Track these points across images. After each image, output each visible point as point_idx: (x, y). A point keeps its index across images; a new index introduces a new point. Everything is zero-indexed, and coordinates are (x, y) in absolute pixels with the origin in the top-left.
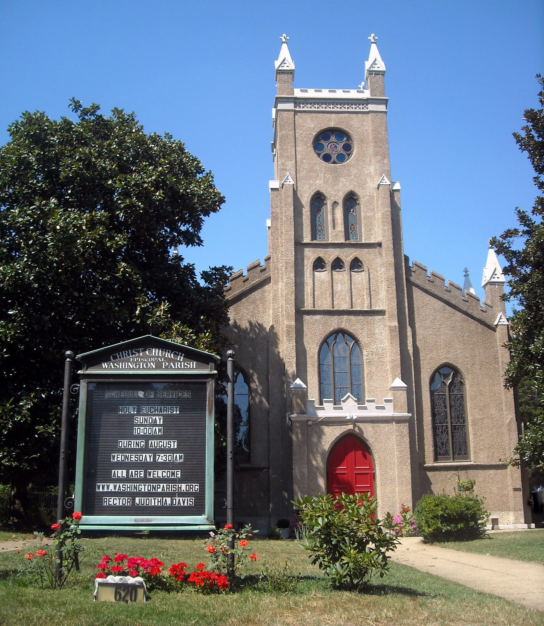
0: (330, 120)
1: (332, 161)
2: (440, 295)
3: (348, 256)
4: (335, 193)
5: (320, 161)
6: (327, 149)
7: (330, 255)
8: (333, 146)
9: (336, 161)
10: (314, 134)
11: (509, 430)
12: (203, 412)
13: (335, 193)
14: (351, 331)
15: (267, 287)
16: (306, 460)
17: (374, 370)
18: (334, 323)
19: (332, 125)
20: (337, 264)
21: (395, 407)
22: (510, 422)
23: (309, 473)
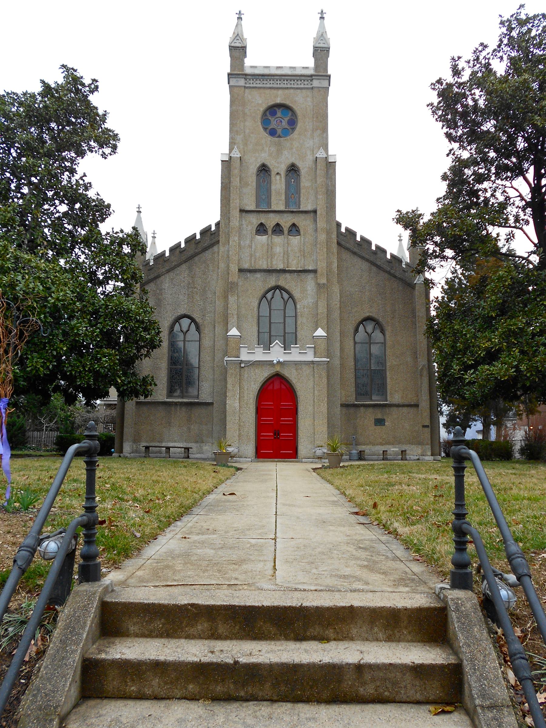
0: (276, 96)
1: (278, 134)
2: (367, 256)
4: (279, 166)
5: (265, 135)
6: (274, 124)
8: (278, 121)
9: (281, 135)
10: (262, 109)
11: (421, 375)
13: (279, 166)
14: (287, 287)
15: (215, 248)
16: (238, 396)
17: (305, 321)
18: (272, 281)
19: (278, 101)
20: (278, 229)
21: (315, 353)
22: (422, 369)
23: (240, 407)
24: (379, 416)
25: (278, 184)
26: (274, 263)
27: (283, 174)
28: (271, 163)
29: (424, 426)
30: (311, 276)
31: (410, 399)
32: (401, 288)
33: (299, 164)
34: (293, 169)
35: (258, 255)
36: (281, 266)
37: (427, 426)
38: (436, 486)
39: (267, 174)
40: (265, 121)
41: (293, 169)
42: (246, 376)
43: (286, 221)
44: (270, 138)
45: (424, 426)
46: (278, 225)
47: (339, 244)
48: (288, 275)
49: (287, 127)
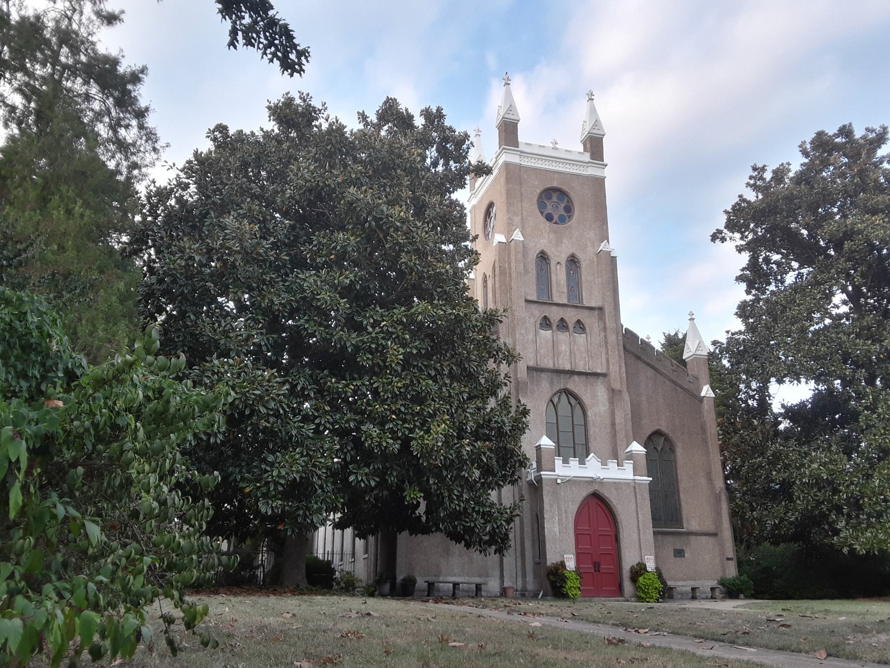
1: (554, 221)
3: (571, 316)
4: (559, 256)
5: (542, 219)
6: (549, 209)
7: (555, 314)
12: (304, 584)
13: (559, 256)
20: (563, 325)
24: (678, 547)
25: (559, 275)
26: (560, 362)
27: (563, 263)
28: (550, 252)
29: (728, 559)
30: (601, 379)
31: (709, 527)
32: (688, 400)
33: (579, 255)
34: (573, 261)
35: (542, 351)
36: (568, 367)
37: (732, 559)
38: (833, 631)
39: (574, 266)
40: (541, 206)
41: (573, 261)
42: (562, 494)
43: (571, 316)
44: (548, 223)
45: (728, 559)
46: (562, 320)
47: (625, 348)
48: (576, 378)
49: (563, 213)
